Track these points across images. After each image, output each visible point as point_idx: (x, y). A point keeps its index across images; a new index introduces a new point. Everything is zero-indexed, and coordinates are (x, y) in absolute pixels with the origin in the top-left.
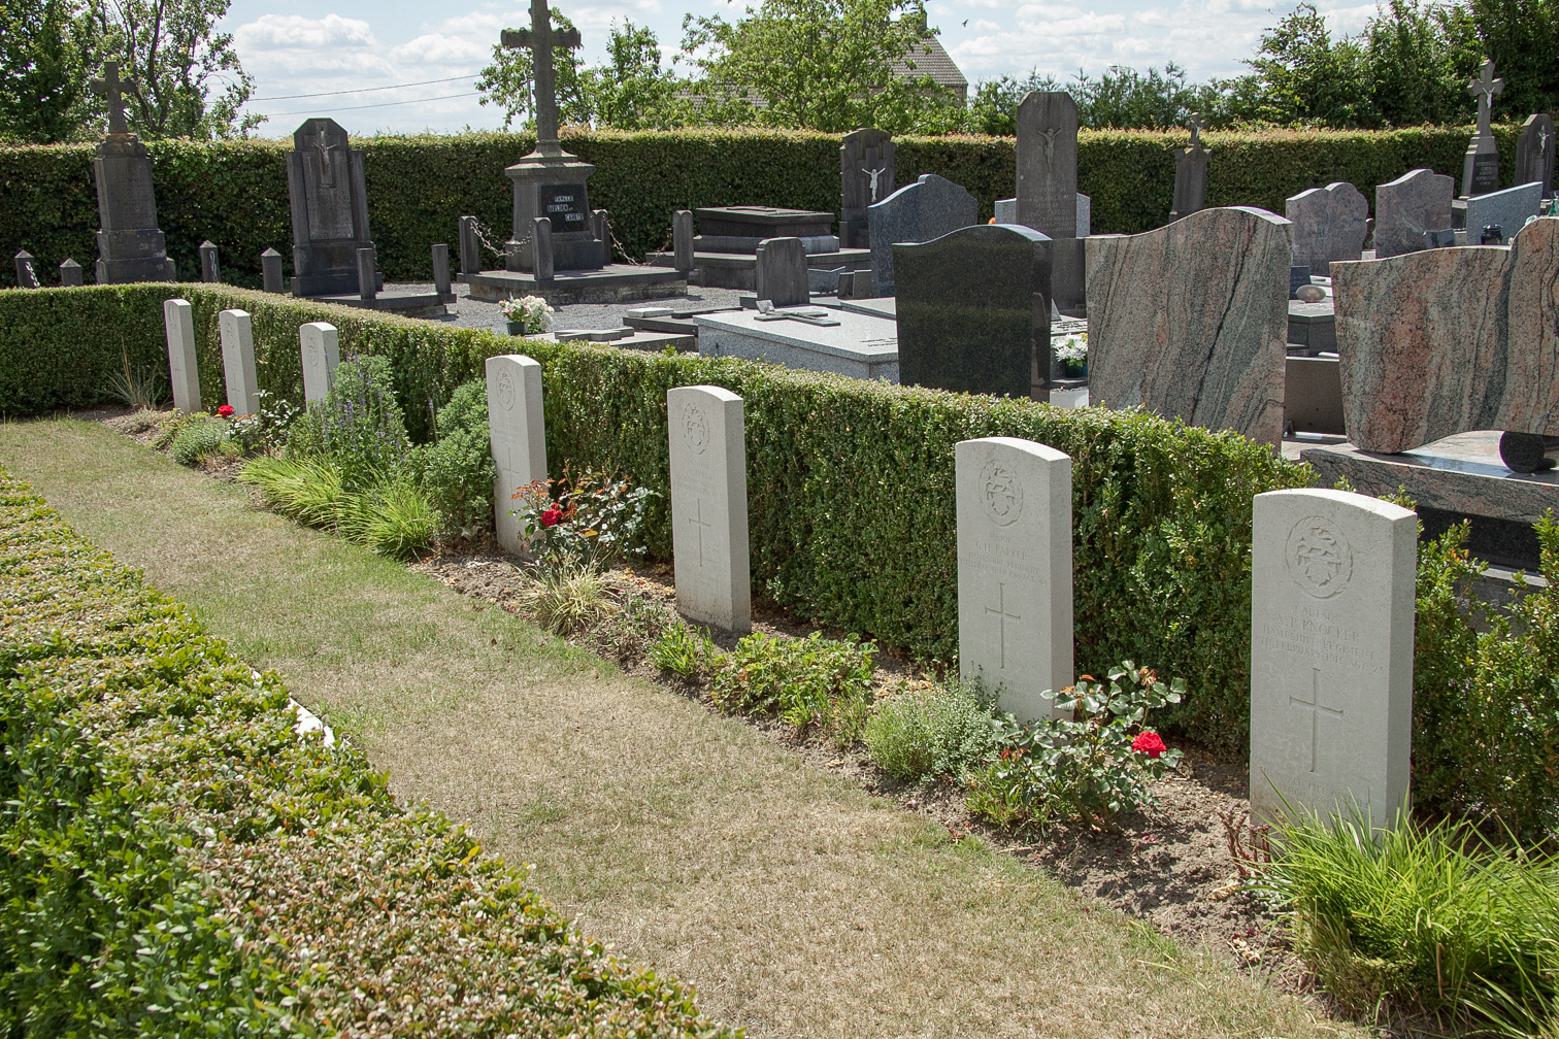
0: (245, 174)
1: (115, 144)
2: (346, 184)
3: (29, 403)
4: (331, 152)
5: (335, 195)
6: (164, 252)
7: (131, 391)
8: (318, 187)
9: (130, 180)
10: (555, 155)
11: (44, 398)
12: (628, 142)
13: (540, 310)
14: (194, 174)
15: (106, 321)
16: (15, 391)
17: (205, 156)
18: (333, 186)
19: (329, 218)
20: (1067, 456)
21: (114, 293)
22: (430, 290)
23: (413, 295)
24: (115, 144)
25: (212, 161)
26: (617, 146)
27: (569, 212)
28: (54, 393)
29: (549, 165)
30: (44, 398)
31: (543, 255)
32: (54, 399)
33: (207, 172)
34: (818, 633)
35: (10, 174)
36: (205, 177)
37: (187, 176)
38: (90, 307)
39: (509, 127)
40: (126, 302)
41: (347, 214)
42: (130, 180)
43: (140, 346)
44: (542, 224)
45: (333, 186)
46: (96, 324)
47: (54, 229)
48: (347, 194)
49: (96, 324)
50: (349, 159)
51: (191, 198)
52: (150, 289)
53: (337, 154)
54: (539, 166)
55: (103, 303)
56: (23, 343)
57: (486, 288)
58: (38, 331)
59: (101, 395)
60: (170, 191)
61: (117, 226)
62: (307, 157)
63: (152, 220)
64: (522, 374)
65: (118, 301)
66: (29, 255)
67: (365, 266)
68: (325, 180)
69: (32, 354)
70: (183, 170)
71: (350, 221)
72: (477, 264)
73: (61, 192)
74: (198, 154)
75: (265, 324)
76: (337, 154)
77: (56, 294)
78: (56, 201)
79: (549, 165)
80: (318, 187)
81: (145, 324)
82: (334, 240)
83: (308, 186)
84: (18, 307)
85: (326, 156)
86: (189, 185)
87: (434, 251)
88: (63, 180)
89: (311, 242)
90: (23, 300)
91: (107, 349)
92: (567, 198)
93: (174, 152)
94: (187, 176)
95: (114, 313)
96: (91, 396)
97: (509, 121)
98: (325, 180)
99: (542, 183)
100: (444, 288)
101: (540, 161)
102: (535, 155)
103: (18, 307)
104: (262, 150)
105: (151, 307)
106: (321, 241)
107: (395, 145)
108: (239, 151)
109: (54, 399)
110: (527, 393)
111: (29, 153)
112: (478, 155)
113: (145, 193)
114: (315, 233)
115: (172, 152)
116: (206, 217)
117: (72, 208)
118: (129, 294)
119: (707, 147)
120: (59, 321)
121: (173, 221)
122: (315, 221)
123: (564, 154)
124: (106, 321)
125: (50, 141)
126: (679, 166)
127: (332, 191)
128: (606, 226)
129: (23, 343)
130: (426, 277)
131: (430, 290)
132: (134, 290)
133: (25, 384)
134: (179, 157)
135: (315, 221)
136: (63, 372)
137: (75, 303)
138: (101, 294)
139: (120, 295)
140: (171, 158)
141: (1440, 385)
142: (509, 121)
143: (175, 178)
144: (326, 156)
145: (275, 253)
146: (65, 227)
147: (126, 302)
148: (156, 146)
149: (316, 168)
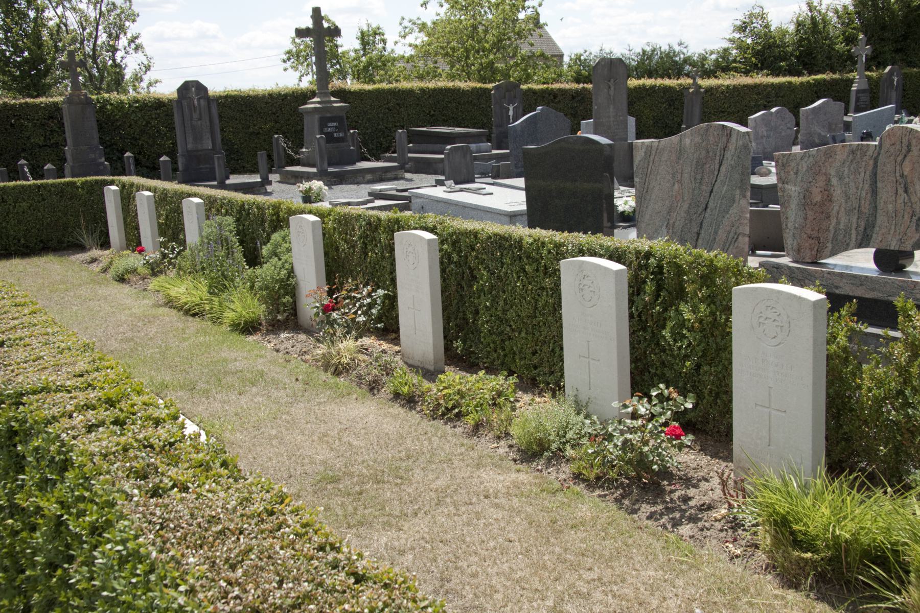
4: (199, 100)
7: (86, 240)
8: (191, 120)
13: (320, 189)
15: (71, 199)
16: (19, 241)
18: (200, 119)
21: (75, 183)
22: (257, 178)
25: (130, 106)
28: (41, 241)
30: (36, 244)
31: (321, 157)
32: (42, 245)
33: (127, 113)
34: (484, 371)
38: (61, 191)
40: (82, 188)
41: (209, 135)
45: (200, 119)
48: (208, 124)
56: (23, 213)
58: (31, 205)
59: (69, 242)
62: (185, 103)
63: (96, 141)
65: (78, 187)
68: (196, 116)
69: (29, 219)
70: (113, 112)
75: (162, 199)
77: (42, 184)
80: (191, 120)
84: (20, 192)
85: (196, 102)
89: (188, 151)
92: (335, 124)
93: (108, 101)
96: (62, 242)
97: (300, 80)
98: (196, 116)
101: (318, 103)
102: (316, 99)
103: (20, 192)
109: (42, 245)
112: (283, 100)
114: (190, 146)
115: (107, 102)
116: (127, 139)
117: (50, 135)
118: (84, 183)
119: (415, 93)
120: (44, 200)
122: (190, 139)
123: (333, 99)
126: (399, 105)
127: (199, 122)
129: (23, 213)
131: (257, 178)
132: (87, 181)
134: (111, 104)
136: (46, 229)
137: (53, 189)
139: (78, 184)
140: (106, 105)
142: (300, 80)
144: (196, 102)
145: (167, 159)
146: (46, 146)
147: (82, 188)
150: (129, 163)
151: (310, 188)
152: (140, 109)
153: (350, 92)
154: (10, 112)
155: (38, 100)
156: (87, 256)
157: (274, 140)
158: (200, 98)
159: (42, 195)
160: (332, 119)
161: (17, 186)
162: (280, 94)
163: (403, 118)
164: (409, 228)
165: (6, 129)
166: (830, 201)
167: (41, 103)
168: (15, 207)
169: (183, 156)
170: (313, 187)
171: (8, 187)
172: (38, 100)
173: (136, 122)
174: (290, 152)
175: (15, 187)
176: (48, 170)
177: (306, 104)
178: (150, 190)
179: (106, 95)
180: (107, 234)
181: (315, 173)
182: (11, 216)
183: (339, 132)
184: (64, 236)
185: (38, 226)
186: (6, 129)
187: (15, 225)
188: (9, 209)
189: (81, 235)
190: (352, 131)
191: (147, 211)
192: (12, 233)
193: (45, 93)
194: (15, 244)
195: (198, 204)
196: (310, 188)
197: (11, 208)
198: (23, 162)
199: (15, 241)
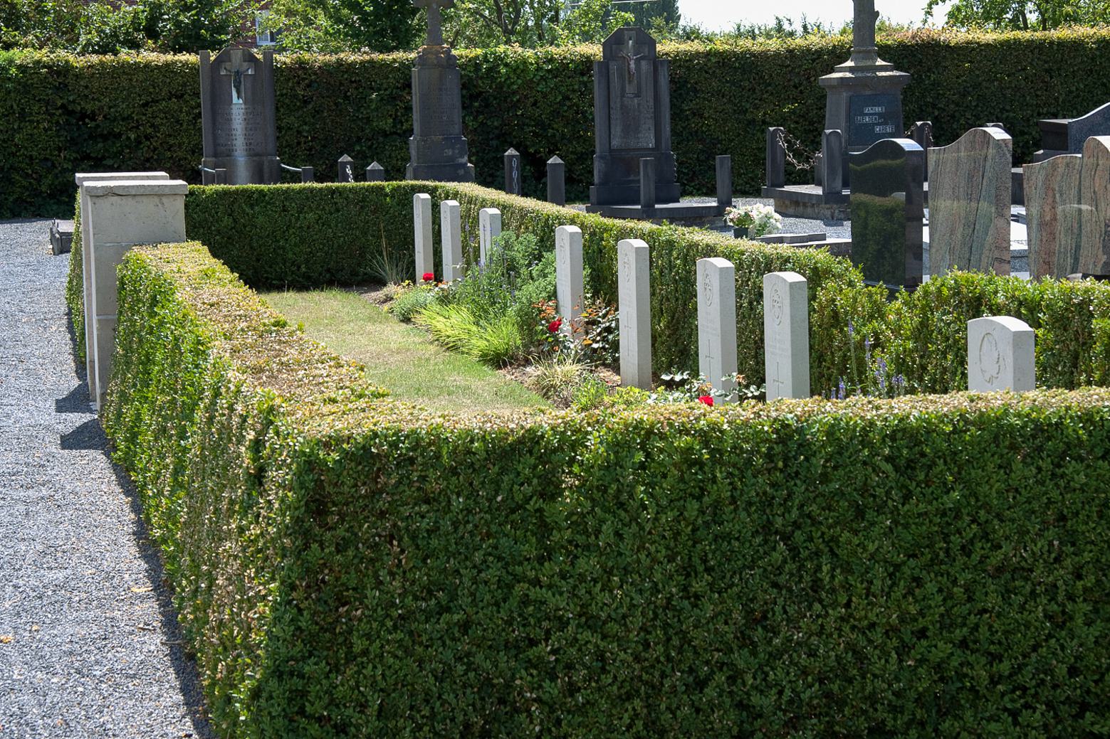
0: (569, 81)
1: (429, 56)
2: (651, 94)
3: (309, 278)
4: (638, 61)
5: (639, 105)
6: (466, 158)
7: (388, 270)
8: (623, 96)
9: (440, 90)
10: (869, 63)
11: (320, 274)
12: (987, 45)
13: (768, 217)
14: (520, 81)
15: (374, 212)
16: (299, 267)
17: (532, 64)
18: (638, 95)
19: (631, 128)
20: (803, 279)
21: (383, 188)
22: (712, 203)
23: (695, 205)
24: (429, 56)
25: (539, 69)
26: (973, 49)
27: (878, 124)
28: (328, 270)
29: (860, 75)
30: (320, 274)
31: (832, 171)
32: (328, 276)
33: (531, 80)
34: (663, 387)
35: (352, 82)
36: (530, 84)
37: (513, 83)
38: (362, 198)
39: (930, 20)
40: (393, 197)
41: (650, 124)
42: (440, 90)
43: (400, 234)
44: (833, 139)
45: (638, 95)
46: (367, 214)
47: (385, 135)
48: (651, 103)
49: (367, 214)
50: (656, 70)
51: (515, 106)
52: (412, 185)
53: (643, 63)
54: (848, 75)
55: (373, 196)
56: (308, 228)
57: (787, 202)
58: (320, 218)
59: (365, 274)
60: (495, 99)
61: (424, 134)
62: (614, 67)
63: (457, 128)
64: (788, 288)
65: (387, 195)
66: (350, 159)
67: (646, 174)
68: (630, 89)
69: (315, 237)
70: (509, 78)
71: (653, 131)
72: (782, 178)
73: (394, 99)
74: (525, 62)
75: (658, 249)
76: (643, 63)
77: (337, 188)
78: (389, 108)
79: (860, 75)
80: (623, 96)
81: (405, 215)
82: (634, 150)
83: (613, 95)
84: (307, 198)
85: (632, 65)
86: (514, 93)
87: (717, 161)
88: (397, 88)
89: (611, 150)
90: (312, 192)
91: (373, 236)
92: (878, 109)
93: (502, 59)
94: (513, 83)
95: (381, 205)
96: (357, 274)
97: (929, 13)
98: (630, 89)
99: (850, 93)
100: (724, 199)
101: (851, 69)
102: (849, 63)
103: (307, 198)
104: (588, 58)
105: (405, 198)
106: (621, 150)
107: (724, 52)
108: (565, 58)
109: (328, 276)
110: (571, 250)
111: (368, 62)
112: (813, 60)
113: (453, 97)
114: (616, 143)
115: (500, 59)
116: (528, 125)
117: (403, 116)
118: (394, 190)
119: (1085, 49)
120: (338, 211)
121: (497, 128)
122: (617, 130)
123: (880, 62)
124: (374, 212)
125: (390, 50)
126: (1048, 71)
127: (636, 101)
128: (928, 138)
129: (308, 228)
130: (711, 192)
131: (712, 203)
132: (399, 187)
133: (307, 261)
134: (506, 65)
135: (617, 130)
136: (337, 253)
137: (351, 196)
138: (372, 189)
139: (387, 190)
140: (498, 65)
141: (1060, 245)
142: (929, 13)
143: (501, 85)
144: (632, 65)
145: (559, 161)
146: (395, 133)
147: (393, 197)
148: (486, 53)
149: (621, 76)
150: (511, 167)
151: (747, 214)
152: (554, 73)
153: (947, 47)
154: (346, 76)
155: (389, 57)
156: (380, 294)
157: (768, 137)
158: (642, 58)
159: (336, 203)
160: (873, 101)
161: (304, 189)
162: (809, 50)
163: (1056, 99)
164: (996, 311)
165: (336, 104)
166: (1056, 220)
167: (395, 61)
168: (298, 219)
169: (601, 157)
170: (754, 214)
171: (293, 190)
172: (389, 57)
173: (545, 96)
174: (790, 158)
175: (301, 191)
176: (372, 171)
177: (832, 71)
178: (729, 257)
179: (501, 48)
180: (412, 263)
181: (818, 196)
182: (291, 231)
183: (885, 123)
184: (359, 265)
185: (326, 248)
186: (336, 104)
187: (295, 245)
188: (290, 221)
189: (382, 266)
190: (919, 123)
191: (716, 299)
192: (290, 255)
193: (408, 43)
194: (293, 273)
195: (723, 270)
196: (747, 214)
197: (293, 220)
198: (346, 158)
199: (294, 269)
